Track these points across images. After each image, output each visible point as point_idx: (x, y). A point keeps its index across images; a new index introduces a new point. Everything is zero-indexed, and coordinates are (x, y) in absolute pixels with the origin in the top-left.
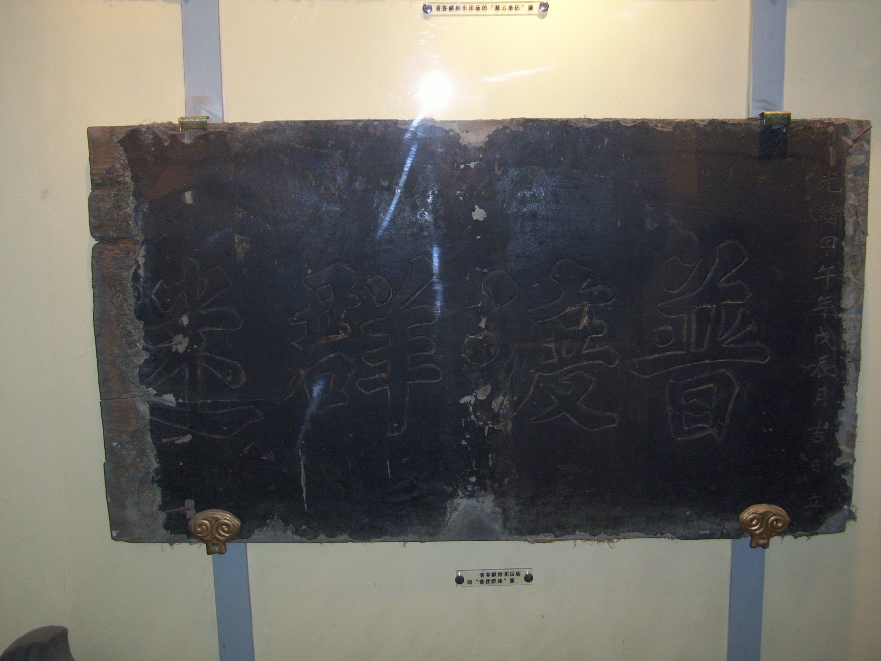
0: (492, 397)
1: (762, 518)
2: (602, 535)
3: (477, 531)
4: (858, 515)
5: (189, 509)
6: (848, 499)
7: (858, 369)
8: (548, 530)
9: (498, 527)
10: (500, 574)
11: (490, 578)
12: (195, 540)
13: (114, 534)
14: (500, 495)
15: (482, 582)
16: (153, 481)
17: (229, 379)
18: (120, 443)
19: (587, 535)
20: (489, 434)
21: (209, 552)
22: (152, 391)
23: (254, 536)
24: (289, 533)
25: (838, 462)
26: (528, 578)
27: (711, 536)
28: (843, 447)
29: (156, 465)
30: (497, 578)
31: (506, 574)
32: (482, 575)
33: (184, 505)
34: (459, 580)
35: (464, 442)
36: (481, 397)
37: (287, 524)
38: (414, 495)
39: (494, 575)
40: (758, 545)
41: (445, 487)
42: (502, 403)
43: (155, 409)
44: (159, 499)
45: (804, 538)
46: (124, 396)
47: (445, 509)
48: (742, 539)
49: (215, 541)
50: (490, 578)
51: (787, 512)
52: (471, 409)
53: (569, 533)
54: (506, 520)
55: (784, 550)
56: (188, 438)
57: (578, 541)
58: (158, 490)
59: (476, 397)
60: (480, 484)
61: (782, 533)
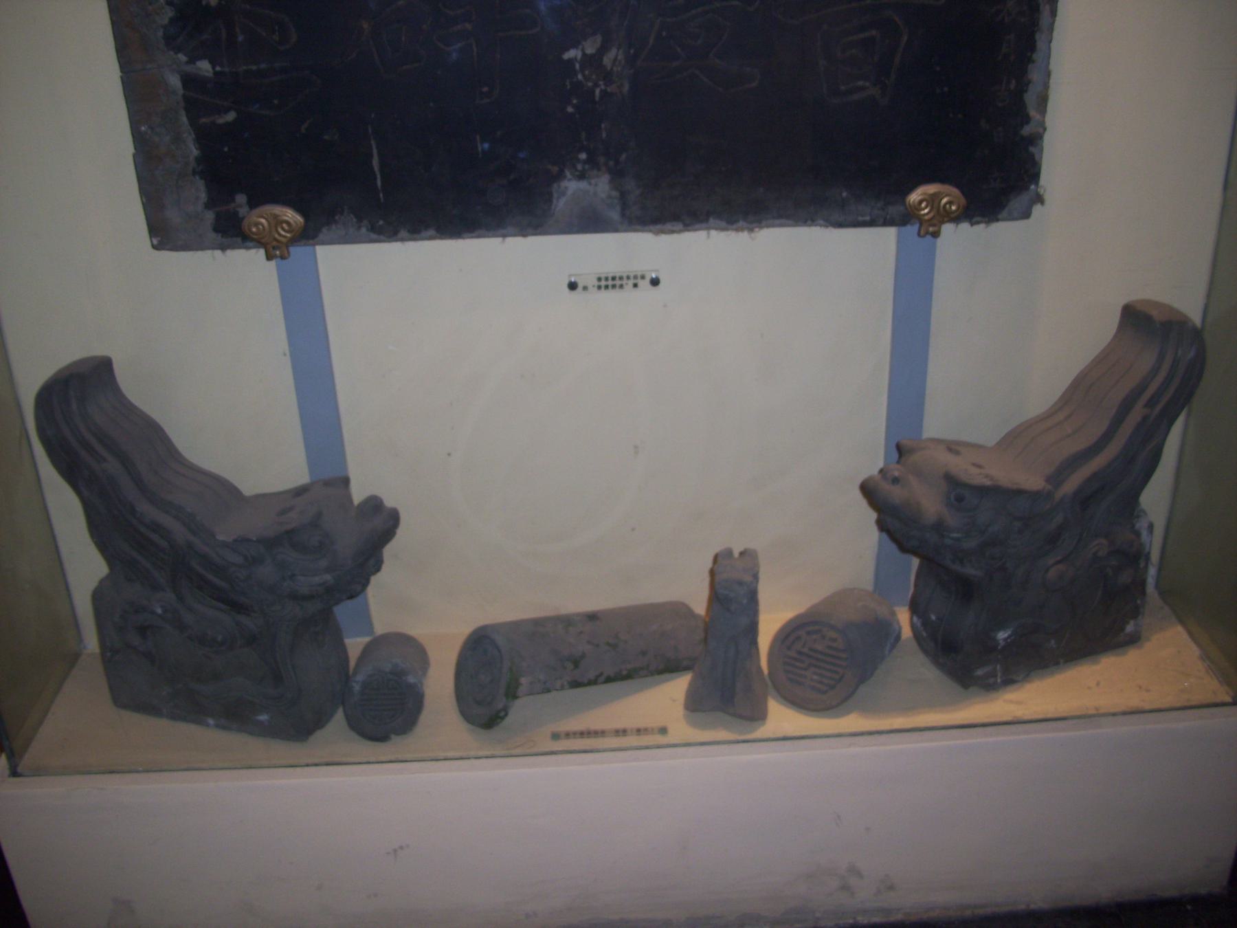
0: (603, 49)
1: (933, 200)
2: (741, 223)
3: (590, 222)
4: (1046, 197)
5: (240, 206)
6: (1035, 177)
7: (1054, 13)
8: (675, 218)
9: (615, 215)
10: (621, 278)
11: (610, 283)
12: (251, 244)
13: (155, 242)
14: (617, 174)
15: (599, 287)
16: (194, 173)
17: (276, 37)
18: (152, 128)
19: (723, 224)
20: (602, 97)
21: (269, 257)
22: (182, 57)
23: (321, 236)
24: (364, 230)
25: (1026, 131)
26: (655, 282)
27: (871, 223)
28: (1033, 113)
29: (195, 152)
30: (618, 282)
31: (628, 278)
32: (599, 279)
33: (233, 200)
34: (573, 286)
35: (570, 109)
36: (589, 51)
37: (360, 219)
38: (512, 177)
39: (614, 279)
40: (927, 233)
41: (550, 167)
42: (615, 59)
43: (190, 81)
44: (203, 196)
45: (982, 226)
46: (149, 66)
47: (551, 194)
48: (909, 227)
49: (275, 243)
50: (610, 283)
51: (963, 192)
52: (577, 66)
53: (701, 222)
54: (624, 206)
55: (957, 239)
56: (231, 116)
57: (713, 232)
58: (201, 184)
59: (583, 50)
60: (592, 161)
61: (956, 219)
